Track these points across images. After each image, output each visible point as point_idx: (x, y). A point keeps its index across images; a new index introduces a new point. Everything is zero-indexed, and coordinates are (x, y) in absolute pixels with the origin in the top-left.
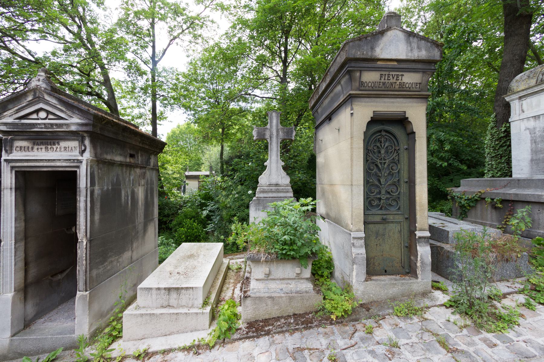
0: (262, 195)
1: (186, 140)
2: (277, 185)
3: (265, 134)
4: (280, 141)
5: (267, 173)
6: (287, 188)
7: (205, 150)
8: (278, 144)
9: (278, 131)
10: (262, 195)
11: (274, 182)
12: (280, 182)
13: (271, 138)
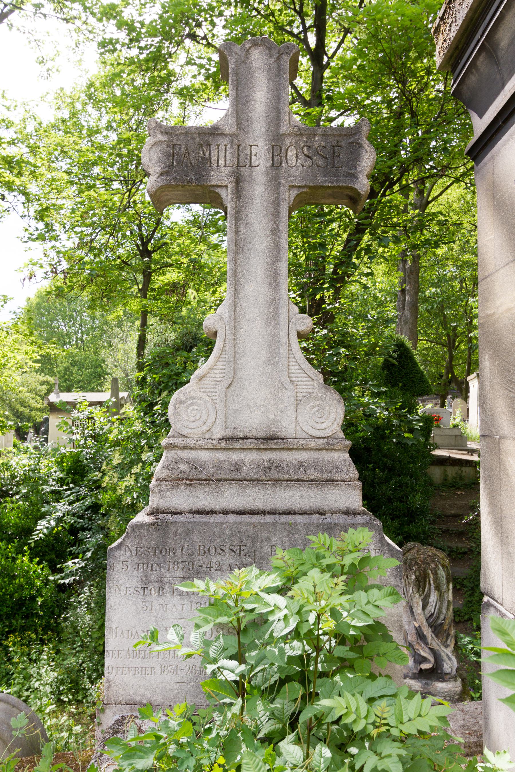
0: (182, 499)
1: (71, 316)
2: (269, 440)
3: (206, 162)
4: (288, 197)
5: (217, 374)
6: (326, 456)
7: (115, 341)
8: (276, 214)
9: (276, 148)
10: (182, 499)
11: (252, 421)
12: (287, 427)
13: (238, 181)
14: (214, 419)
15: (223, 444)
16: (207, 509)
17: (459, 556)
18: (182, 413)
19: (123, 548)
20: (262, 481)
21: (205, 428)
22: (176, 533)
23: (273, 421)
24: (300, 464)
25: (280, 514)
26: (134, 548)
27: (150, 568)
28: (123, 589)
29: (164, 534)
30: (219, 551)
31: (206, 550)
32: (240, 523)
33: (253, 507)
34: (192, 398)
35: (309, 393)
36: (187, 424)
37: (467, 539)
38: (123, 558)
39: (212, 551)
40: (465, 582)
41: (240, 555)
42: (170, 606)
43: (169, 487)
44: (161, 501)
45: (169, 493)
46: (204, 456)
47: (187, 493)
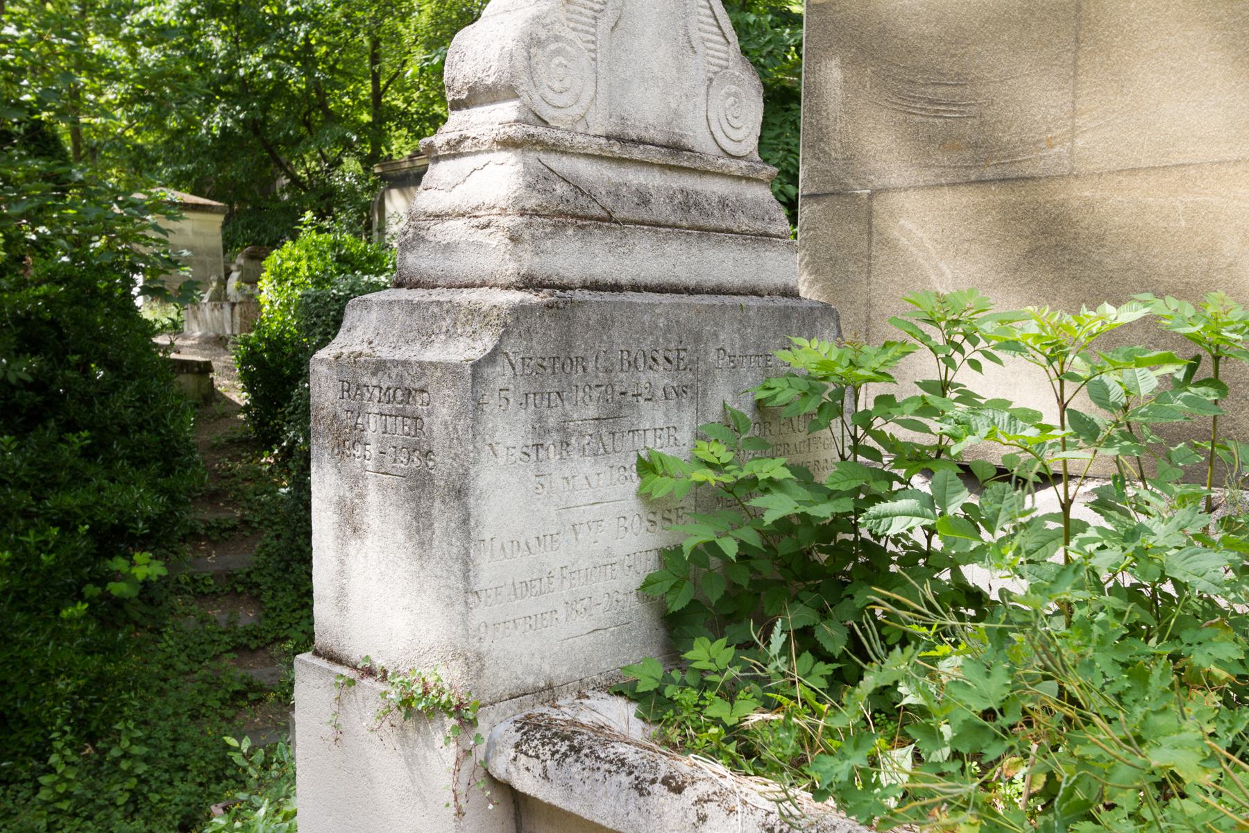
14: (592, 93)
15: (617, 149)
16: (610, 280)
17: (225, 535)
18: (541, 69)
19: (502, 360)
20: (680, 227)
21: (576, 111)
22: (588, 325)
23: (676, 113)
24: (723, 203)
25: (707, 293)
26: (519, 358)
27: (546, 403)
28: (500, 449)
29: (569, 326)
30: (650, 362)
31: (632, 359)
32: (679, 305)
33: (673, 280)
34: (557, 38)
35: (721, 67)
36: (550, 95)
37: (228, 503)
38: (501, 382)
39: (641, 362)
40: (255, 578)
41: (678, 369)
42: (580, 480)
43: (548, 230)
44: (537, 259)
45: (549, 243)
46: (586, 170)
47: (579, 244)
